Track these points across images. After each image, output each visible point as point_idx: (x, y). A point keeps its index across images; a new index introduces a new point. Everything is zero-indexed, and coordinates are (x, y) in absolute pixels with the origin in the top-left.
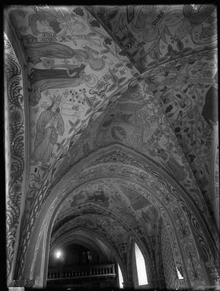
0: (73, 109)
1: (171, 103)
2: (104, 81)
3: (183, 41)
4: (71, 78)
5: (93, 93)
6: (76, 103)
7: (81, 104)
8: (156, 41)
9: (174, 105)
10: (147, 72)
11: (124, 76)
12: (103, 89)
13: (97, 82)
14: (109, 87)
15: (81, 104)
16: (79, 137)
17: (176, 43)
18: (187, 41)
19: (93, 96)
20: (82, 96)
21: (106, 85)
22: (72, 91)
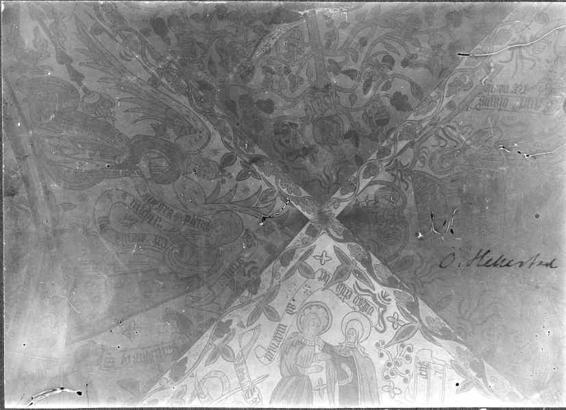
0: (426, 377)
1: (387, 102)
2: (352, 299)
3: (217, 159)
4: (355, 378)
5: (384, 323)
6: (411, 367)
7: (413, 355)
8: (239, 208)
9: (391, 92)
10: (300, 209)
11: (331, 252)
12: (370, 299)
13: (358, 315)
14: (364, 287)
15: (413, 355)
16: (488, 366)
17: (228, 169)
18: (215, 152)
19: (389, 324)
20: (393, 349)
21: (358, 291)
22: (385, 374)
